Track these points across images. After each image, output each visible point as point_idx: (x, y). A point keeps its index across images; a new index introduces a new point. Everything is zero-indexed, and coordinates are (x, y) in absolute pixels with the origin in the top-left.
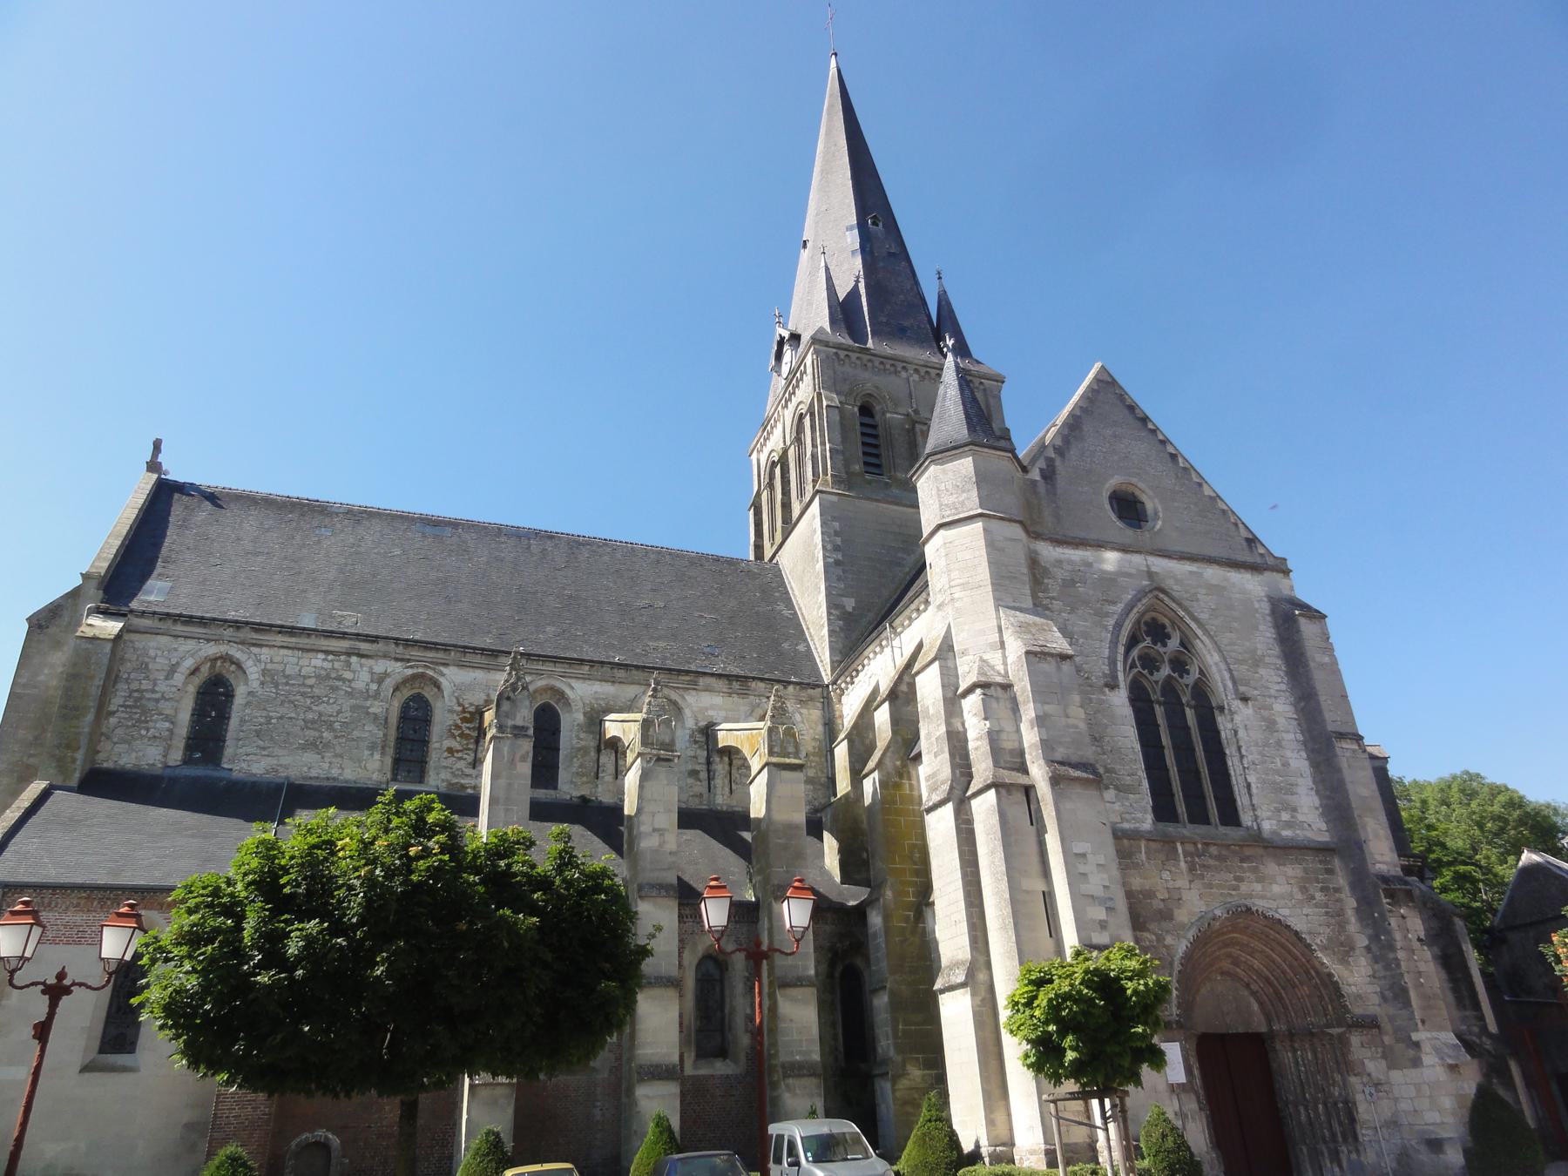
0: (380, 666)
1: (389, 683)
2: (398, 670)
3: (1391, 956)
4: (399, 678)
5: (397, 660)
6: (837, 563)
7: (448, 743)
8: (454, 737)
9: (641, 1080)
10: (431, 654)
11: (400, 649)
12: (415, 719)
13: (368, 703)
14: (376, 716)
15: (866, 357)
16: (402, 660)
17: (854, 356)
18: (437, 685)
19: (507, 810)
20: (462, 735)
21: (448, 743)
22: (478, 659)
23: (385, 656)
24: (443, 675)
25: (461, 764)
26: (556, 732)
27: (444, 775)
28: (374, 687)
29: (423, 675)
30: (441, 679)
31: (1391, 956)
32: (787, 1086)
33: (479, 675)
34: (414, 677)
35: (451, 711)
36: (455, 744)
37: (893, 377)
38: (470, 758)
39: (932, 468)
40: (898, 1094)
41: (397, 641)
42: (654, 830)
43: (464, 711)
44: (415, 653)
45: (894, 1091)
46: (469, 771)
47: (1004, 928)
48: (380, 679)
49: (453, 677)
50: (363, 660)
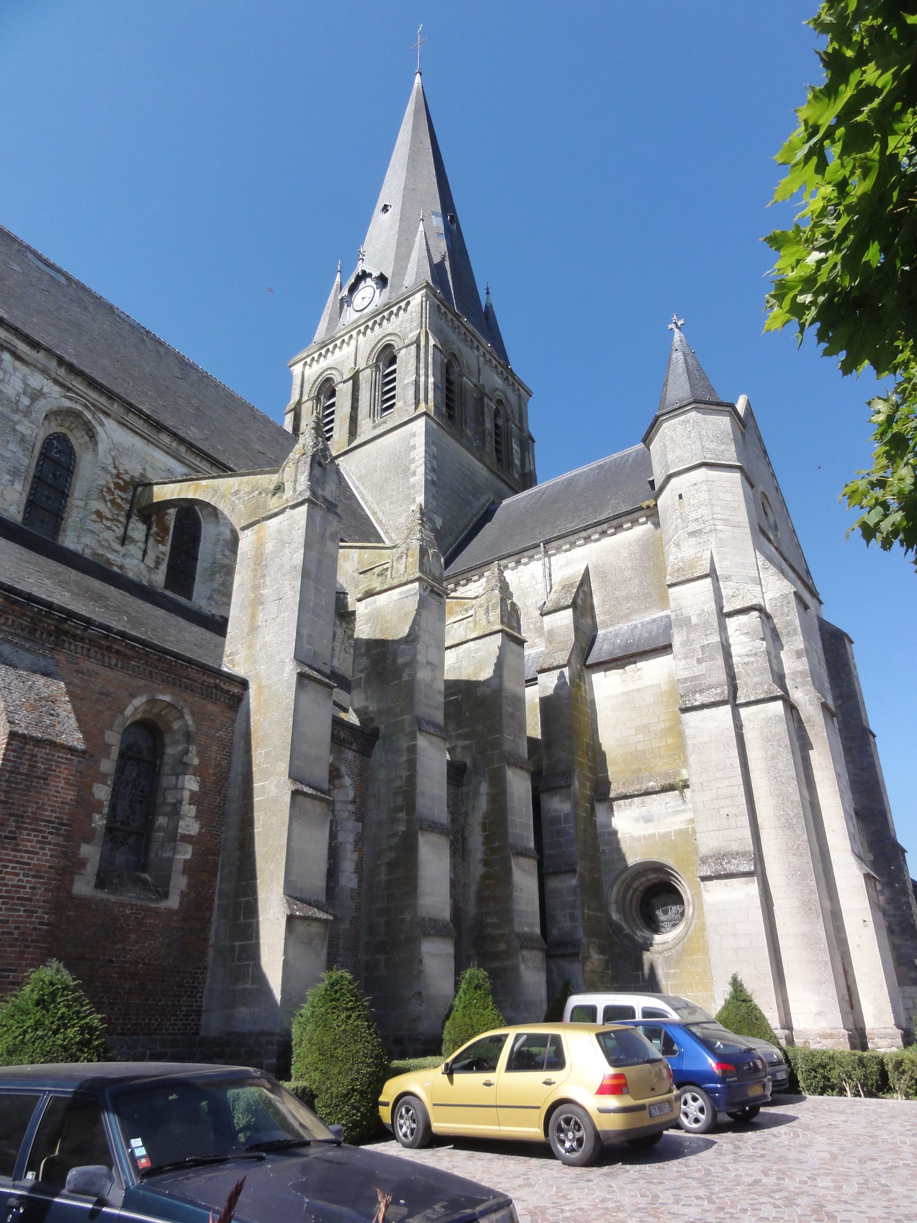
0: (37, 381)
1: (43, 406)
2: (55, 397)
3: (903, 900)
4: (54, 406)
5: (56, 382)
6: (433, 483)
7: (96, 505)
8: (104, 498)
9: (427, 935)
10: (93, 395)
11: (62, 371)
12: (57, 463)
13: (17, 417)
14: (23, 439)
15: (457, 323)
16: (62, 385)
17: (450, 316)
18: (92, 434)
19: (317, 589)
20: (113, 502)
21: (96, 505)
22: (140, 425)
23: (44, 371)
24: (102, 424)
25: (108, 535)
26: (195, 539)
27: (88, 540)
28: (26, 401)
29: (78, 415)
30: (99, 429)
31: (903, 900)
32: (523, 957)
33: (137, 442)
34: (70, 412)
35: (104, 469)
36: (105, 509)
37: (469, 349)
38: (120, 532)
39: (693, 414)
40: (586, 976)
41: (61, 361)
42: (428, 663)
43: (118, 476)
44: (77, 384)
45: (584, 971)
46: (117, 546)
47: (788, 826)
48: (36, 396)
49: (111, 433)
50: (18, 364)
